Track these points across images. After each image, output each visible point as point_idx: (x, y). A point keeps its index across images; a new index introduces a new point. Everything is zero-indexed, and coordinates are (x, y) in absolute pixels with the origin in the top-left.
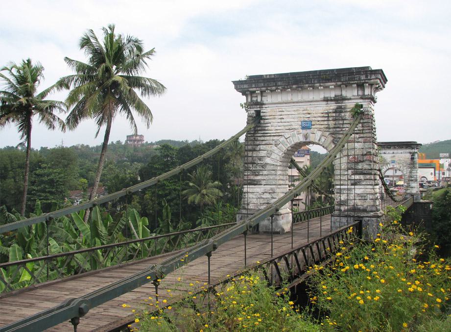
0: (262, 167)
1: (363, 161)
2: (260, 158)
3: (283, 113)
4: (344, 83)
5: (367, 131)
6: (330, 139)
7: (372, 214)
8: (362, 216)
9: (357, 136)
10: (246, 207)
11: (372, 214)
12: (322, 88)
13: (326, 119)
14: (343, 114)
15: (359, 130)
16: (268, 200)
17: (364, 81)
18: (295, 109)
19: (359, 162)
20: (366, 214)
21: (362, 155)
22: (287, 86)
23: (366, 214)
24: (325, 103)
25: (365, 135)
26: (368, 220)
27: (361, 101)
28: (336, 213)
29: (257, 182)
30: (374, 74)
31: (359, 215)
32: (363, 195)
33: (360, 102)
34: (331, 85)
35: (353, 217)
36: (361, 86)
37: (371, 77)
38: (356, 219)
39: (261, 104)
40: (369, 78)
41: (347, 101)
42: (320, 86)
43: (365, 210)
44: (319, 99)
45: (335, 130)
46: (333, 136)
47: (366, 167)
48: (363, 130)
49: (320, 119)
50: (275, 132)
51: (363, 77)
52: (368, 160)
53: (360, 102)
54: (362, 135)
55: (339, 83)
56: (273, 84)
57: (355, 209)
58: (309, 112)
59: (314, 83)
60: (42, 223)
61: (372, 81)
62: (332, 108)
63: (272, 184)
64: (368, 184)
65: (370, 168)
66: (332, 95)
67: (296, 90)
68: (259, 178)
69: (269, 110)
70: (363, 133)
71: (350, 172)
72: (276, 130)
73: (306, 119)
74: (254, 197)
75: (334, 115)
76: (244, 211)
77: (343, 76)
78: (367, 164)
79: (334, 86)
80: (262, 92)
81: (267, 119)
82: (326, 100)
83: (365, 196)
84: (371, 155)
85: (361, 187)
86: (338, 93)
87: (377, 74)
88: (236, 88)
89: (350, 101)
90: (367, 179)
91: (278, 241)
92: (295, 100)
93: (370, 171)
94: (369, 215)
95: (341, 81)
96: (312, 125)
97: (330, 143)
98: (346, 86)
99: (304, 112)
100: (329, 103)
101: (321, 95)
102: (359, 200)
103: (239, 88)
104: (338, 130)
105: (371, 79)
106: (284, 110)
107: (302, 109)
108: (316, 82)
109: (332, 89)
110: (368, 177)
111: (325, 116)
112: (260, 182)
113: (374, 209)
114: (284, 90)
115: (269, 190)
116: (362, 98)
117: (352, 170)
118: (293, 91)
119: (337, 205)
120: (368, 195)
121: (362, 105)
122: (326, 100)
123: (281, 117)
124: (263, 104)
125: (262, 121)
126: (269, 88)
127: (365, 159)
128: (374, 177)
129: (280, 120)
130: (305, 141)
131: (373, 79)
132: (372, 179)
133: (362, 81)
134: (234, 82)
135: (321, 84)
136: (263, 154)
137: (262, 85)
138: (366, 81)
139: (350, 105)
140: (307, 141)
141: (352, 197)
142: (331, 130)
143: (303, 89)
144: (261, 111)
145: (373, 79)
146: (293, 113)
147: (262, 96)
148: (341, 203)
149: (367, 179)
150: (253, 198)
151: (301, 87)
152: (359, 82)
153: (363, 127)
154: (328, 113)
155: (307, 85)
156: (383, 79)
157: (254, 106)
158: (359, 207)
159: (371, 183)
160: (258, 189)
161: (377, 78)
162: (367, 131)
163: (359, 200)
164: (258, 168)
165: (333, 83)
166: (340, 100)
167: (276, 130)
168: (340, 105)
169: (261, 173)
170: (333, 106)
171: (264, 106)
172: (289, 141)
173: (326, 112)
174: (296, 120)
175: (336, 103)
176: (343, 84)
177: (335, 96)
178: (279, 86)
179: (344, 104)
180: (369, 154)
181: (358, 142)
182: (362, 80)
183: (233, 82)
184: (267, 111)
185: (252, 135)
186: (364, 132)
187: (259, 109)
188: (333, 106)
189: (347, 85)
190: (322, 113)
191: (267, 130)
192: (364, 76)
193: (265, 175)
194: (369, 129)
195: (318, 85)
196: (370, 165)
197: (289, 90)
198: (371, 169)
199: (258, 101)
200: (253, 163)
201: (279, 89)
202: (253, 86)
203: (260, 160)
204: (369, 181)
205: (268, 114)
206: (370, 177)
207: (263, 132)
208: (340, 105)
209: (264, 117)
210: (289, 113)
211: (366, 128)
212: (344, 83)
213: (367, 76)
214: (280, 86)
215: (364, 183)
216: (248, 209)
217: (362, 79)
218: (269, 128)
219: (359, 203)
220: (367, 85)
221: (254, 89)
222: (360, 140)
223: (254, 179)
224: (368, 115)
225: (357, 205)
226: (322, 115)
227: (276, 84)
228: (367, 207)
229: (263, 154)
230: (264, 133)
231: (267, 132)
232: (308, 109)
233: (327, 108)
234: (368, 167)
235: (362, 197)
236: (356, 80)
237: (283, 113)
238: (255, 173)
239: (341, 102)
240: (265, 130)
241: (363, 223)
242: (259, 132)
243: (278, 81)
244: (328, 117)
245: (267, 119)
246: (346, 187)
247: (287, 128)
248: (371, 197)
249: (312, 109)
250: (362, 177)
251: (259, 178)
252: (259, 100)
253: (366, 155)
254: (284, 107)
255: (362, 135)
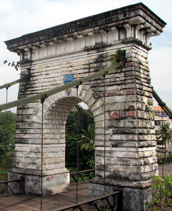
0: (30, 126)
1: (125, 118)
2: (28, 116)
3: (48, 69)
4: (102, 27)
5: (129, 81)
6: (91, 92)
7: (135, 183)
8: (122, 185)
9: (119, 87)
10: (16, 166)
11: (135, 183)
12: (81, 36)
13: (87, 70)
14: (104, 64)
15: (121, 80)
16: (34, 160)
17: (122, 22)
18: (59, 63)
19: (121, 119)
20: (127, 184)
21: (125, 110)
22: (48, 39)
23: (127, 184)
24: (86, 53)
25: (127, 86)
26: (130, 192)
27: (124, 46)
28: (96, 179)
29: (25, 141)
30: (133, 10)
31: (120, 183)
32: (124, 159)
33: (122, 47)
34: (89, 31)
35: (113, 185)
36: (121, 29)
37: (129, 15)
38: (116, 188)
39: (30, 62)
40: (128, 16)
41: (108, 49)
42: (79, 34)
43: (127, 179)
44: (80, 50)
45: (96, 82)
46: (94, 89)
47: (128, 124)
48: (125, 80)
49: (81, 71)
50: (40, 88)
51: (121, 17)
52: (131, 116)
53: (122, 47)
54: (124, 87)
55: (97, 28)
56: (36, 39)
57: (116, 176)
58: (71, 65)
59: (72, 32)
60: (152, 105)
61: (132, 19)
62: (93, 58)
63: (37, 143)
64: (131, 145)
65: (133, 126)
66: (92, 43)
67: (57, 43)
68: (26, 136)
69: (37, 67)
70: (125, 84)
71: (110, 131)
72: (42, 86)
73: (68, 73)
74: (23, 155)
75: (95, 65)
76: (14, 170)
77: (100, 19)
78: (129, 121)
79: (94, 33)
80: (31, 50)
81: (35, 76)
82: (87, 50)
83: (127, 161)
84: (134, 110)
85: (123, 149)
86: (99, 40)
87: (136, 9)
88: (9, 48)
89: (111, 48)
90: (130, 140)
91: (63, 198)
92: (59, 53)
93: (133, 130)
94: (131, 185)
95: (98, 26)
96: (74, 79)
97: (90, 99)
98: (107, 31)
99: (68, 65)
100: (90, 53)
101: (82, 45)
102: (121, 165)
103: (10, 48)
104: (99, 82)
105: (131, 18)
106: (49, 65)
107: (65, 63)
108: (74, 30)
109: (91, 36)
110: (131, 137)
111: (86, 67)
112: (27, 140)
113: (138, 177)
114: (47, 46)
115: (35, 150)
116: (123, 42)
117: (114, 129)
118: (57, 44)
119: (97, 170)
120: (131, 160)
121: (125, 51)
122: (87, 50)
123: (47, 72)
124: (32, 61)
125: (31, 79)
126: (34, 44)
127: (127, 115)
128: (138, 138)
129: (45, 76)
130: (67, 96)
131: (133, 17)
132: (135, 140)
133: (120, 22)
134: (6, 42)
135: (80, 32)
136: (30, 111)
137: (28, 41)
138: (125, 21)
139: (111, 51)
140: (70, 96)
141: (113, 161)
142: (92, 82)
143: (65, 41)
144: (31, 68)
145: (133, 17)
146: (57, 67)
147: (31, 54)
148: (104, 168)
149: (130, 140)
150: (22, 157)
151: (62, 39)
152: (117, 23)
153: (125, 76)
154: (89, 64)
155: (66, 36)
156: (148, 15)
157: (25, 65)
158: (121, 173)
159: (134, 145)
160: (26, 148)
161: (137, 15)
162: (129, 81)
163: (121, 165)
164: (26, 127)
165: (91, 29)
166: (101, 48)
167: (42, 86)
168: (101, 53)
169: (28, 132)
170: (94, 55)
171: (33, 64)
172: (52, 97)
173: (88, 63)
174: (59, 75)
175: (97, 52)
176: (101, 29)
177: (96, 44)
178: (41, 40)
179: (104, 53)
180: (131, 109)
181: (120, 95)
182: (121, 20)
183: (4, 42)
184: (36, 68)
185: (23, 93)
186: (127, 82)
187: (29, 67)
188: (94, 55)
189: (107, 30)
190: (84, 65)
191: (35, 87)
192: (122, 14)
193: (32, 134)
194: (133, 79)
195: (76, 33)
196: (133, 122)
197: (51, 43)
198: (135, 128)
199: (28, 59)
200: (23, 121)
201: (43, 44)
202: (21, 44)
203: (28, 119)
204: (131, 142)
205: (36, 71)
206: (133, 137)
207: (31, 89)
208: (101, 53)
209: (32, 75)
210: (54, 68)
211: (128, 78)
212: (102, 27)
213: (125, 15)
214: (43, 40)
215: (126, 145)
216: (18, 168)
217: (120, 19)
218: (37, 85)
219: (121, 169)
220: (127, 25)
221: (22, 47)
222: (122, 92)
223: (22, 137)
224: (131, 61)
225: (118, 171)
226: (84, 67)
227: (39, 39)
228: (130, 174)
229: (30, 111)
230: (32, 91)
231: (35, 89)
232: (71, 61)
233: (89, 58)
234: (131, 125)
235: (123, 161)
236: (114, 22)
237: (48, 69)
238: (23, 131)
239: (102, 50)
240: (33, 87)
241: (124, 194)
242: (29, 90)
243: (41, 35)
244: (89, 68)
245: (35, 76)
246: (103, 149)
247: (51, 83)
248: (134, 162)
249: (74, 61)
250: (124, 137)
251: (26, 136)
252: (29, 58)
253: (128, 110)
254: (50, 62)
255: (124, 87)
